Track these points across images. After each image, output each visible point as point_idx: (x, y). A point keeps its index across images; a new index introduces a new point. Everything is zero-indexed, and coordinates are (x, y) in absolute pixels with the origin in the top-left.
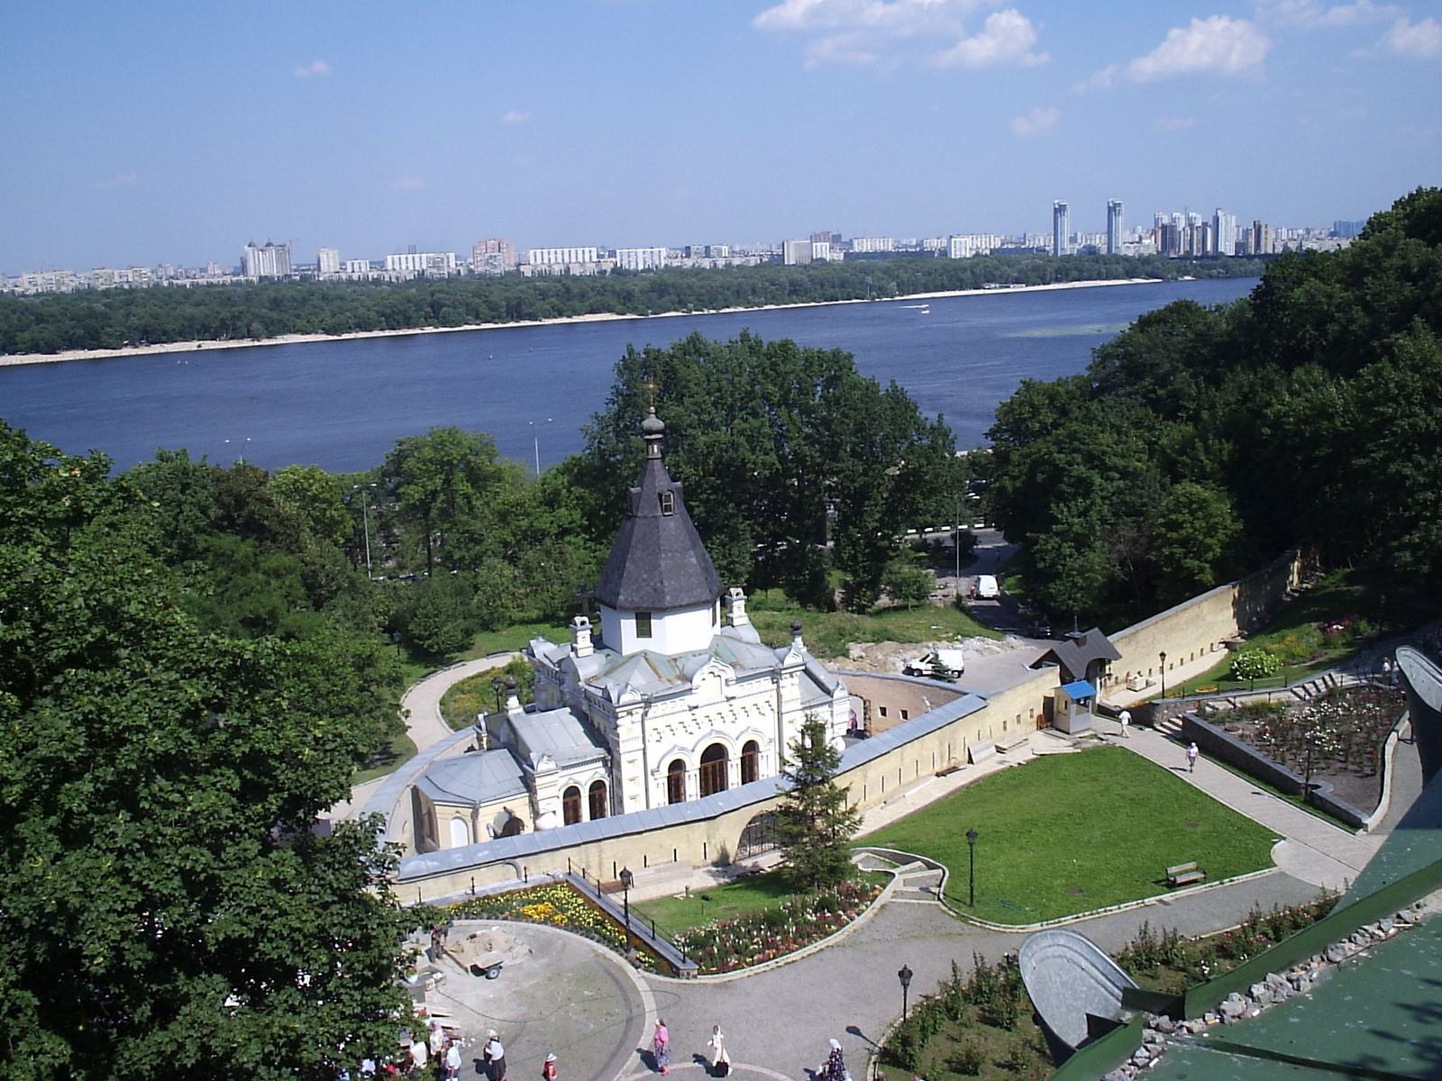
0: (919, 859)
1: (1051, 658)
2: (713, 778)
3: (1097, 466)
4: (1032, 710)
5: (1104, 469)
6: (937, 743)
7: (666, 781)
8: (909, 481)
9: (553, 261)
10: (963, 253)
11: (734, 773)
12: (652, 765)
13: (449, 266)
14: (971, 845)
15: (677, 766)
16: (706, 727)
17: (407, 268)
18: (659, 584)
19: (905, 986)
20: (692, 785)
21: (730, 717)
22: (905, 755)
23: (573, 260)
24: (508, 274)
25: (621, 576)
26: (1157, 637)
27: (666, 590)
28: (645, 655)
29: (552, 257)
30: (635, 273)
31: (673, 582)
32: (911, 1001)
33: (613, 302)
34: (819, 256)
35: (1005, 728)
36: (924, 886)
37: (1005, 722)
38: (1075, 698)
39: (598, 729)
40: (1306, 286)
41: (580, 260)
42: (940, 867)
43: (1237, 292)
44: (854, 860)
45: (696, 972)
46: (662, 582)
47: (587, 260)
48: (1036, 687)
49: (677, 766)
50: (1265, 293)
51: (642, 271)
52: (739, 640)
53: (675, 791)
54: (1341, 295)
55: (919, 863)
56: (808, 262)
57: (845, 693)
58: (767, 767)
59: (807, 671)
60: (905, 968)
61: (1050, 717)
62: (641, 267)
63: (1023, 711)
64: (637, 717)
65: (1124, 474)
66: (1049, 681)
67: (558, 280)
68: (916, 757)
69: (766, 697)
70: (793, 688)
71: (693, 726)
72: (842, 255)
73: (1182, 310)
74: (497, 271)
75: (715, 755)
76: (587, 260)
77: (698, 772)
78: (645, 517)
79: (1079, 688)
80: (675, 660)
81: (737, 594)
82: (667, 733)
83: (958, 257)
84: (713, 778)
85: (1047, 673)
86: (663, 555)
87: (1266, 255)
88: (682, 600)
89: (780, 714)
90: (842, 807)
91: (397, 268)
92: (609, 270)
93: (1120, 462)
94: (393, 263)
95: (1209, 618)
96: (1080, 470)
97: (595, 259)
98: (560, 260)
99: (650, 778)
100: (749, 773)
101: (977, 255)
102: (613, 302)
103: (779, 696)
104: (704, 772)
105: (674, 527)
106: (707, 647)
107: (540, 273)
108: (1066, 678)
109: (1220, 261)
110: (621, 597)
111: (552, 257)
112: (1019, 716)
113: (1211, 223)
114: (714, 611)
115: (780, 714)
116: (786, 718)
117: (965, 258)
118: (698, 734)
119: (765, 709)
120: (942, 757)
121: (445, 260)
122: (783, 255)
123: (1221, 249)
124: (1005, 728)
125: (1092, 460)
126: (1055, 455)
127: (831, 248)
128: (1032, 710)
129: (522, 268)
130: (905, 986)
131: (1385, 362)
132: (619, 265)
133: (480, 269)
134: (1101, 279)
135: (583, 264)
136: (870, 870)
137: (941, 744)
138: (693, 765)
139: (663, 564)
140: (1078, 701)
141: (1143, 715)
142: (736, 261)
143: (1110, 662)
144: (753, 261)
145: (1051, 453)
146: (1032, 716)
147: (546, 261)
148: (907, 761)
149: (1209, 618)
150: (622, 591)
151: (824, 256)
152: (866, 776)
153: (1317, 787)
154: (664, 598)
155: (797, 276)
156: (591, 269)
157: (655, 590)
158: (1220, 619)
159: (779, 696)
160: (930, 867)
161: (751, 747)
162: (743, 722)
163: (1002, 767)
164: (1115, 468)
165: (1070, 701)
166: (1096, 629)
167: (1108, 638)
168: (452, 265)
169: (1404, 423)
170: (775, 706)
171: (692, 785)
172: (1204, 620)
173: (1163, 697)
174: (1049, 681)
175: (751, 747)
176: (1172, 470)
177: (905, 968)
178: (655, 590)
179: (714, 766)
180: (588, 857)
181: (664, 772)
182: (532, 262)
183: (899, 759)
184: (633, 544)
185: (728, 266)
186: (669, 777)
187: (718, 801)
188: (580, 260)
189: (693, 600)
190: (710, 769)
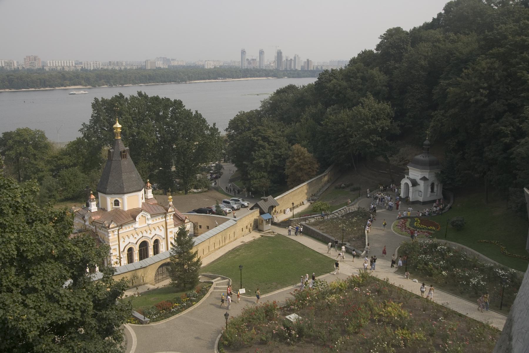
0: (220, 277)
1: (256, 206)
2: (143, 254)
3: (267, 141)
5: (269, 142)
6: (221, 236)
7: (126, 255)
8: (201, 149)
9: (57, 65)
11: (151, 252)
12: (122, 250)
13: (14, 66)
14: (241, 270)
15: (130, 250)
16: (140, 235)
17: (72, 65)
18: (122, 185)
20: (136, 257)
21: (149, 232)
23: (65, 65)
24: (39, 69)
25: (107, 182)
27: (124, 186)
29: (57, 63)
30: (90, 71)
32: (229, 321)
33: (83, 82)
34: (159, 66)
35: (242, 231)
38: (265, 219)
41: (68, 65)
42: (227, 279)
45: (149, 322)
46: (123, 184)
47: (71, 65)
48: (252, 216)
49: (130, 250)
50: (319, 83)
53: (130, 259)
54: (345, 84)
55: (219, 278)
56: (155, 68)
58: (162, 248)
61: (257, 226)
62: (92, 68)
64: (116, 233)
66: (256, 214)
67: (60, 72)
68: (214, 242)
69: (162, 223)
72: (167, 66)
73: (291, 88)
74: (35, 68)
75: (144, 245)
76: (71, 65)
77: (138, 251)
78: (116, 160)
82: (127, 238)
83: (208, 68)
84: (143, 254)
85: (256, 211)
86: (123, 174)
87: (311, 71)
88: (130, 190)
90: (195, 259)
91: (63, 65)
92: (80, 69)
93: (274, 140)
94: (64, 63)
96: (261, 142)
97: (74, 65)
98: (60, 65)
100: (156, 251)
101: (215, 68)
103: (166, 223)
104: (140, 251)
107: (52, 69)
108: (262, 213)
109: (296, 72)
110: (108, 190)
111: (57, 63)
113: (293, 59)
115: (167, 229)
116: (169, 230)
117: (211, 68)
118: (138, 238)
119: (161, 228)
121: (12, 63)
122: (146, 65)
123: (297, 68)
124: (242, 231)
125: (265, 139)
126: (253, 137)
127: (163, 64)
128: (251, 224)
129: (45, 68)
131: (360, 106)
132: (83, 67)
133: (27, 67)
134: (255, 77)
135: (69, 67)
136: (203, 281)
137: (222, 237)
140: (266, 220)
142: (128, 68)
143: (275, 206)
144: (134, 68)
145: (251, 137)
146: (251, 226)
147: (54, 65)
148: (211, 243)
150: (108, 187)
151: (161, 66)
154: (124, 189)
156: (72, 69)
157: (120, 187)
159: (166, 223)
160: (224, 279)
161: (156, 242)
162: (153, 233)
163: (243, 243)
164: (272, 142)
165: (263, 221)
166: (271, 196)
167: (275, 198)
168: (16, 65)
169: (366, 127)
170: (165, 227)
171: (136, 257)
173: (293, 218)
174: (256, 214)
175: (156, 242)
178: (120, 187)
179: (144, 249)
180: (207, 253)
182: (49, 65)
183: (208, 243)
184: (111, 170)
186: (128, 254)
187: (146, 262)
188: (68, 65)
189: (134, 190)
190: (145, 249)
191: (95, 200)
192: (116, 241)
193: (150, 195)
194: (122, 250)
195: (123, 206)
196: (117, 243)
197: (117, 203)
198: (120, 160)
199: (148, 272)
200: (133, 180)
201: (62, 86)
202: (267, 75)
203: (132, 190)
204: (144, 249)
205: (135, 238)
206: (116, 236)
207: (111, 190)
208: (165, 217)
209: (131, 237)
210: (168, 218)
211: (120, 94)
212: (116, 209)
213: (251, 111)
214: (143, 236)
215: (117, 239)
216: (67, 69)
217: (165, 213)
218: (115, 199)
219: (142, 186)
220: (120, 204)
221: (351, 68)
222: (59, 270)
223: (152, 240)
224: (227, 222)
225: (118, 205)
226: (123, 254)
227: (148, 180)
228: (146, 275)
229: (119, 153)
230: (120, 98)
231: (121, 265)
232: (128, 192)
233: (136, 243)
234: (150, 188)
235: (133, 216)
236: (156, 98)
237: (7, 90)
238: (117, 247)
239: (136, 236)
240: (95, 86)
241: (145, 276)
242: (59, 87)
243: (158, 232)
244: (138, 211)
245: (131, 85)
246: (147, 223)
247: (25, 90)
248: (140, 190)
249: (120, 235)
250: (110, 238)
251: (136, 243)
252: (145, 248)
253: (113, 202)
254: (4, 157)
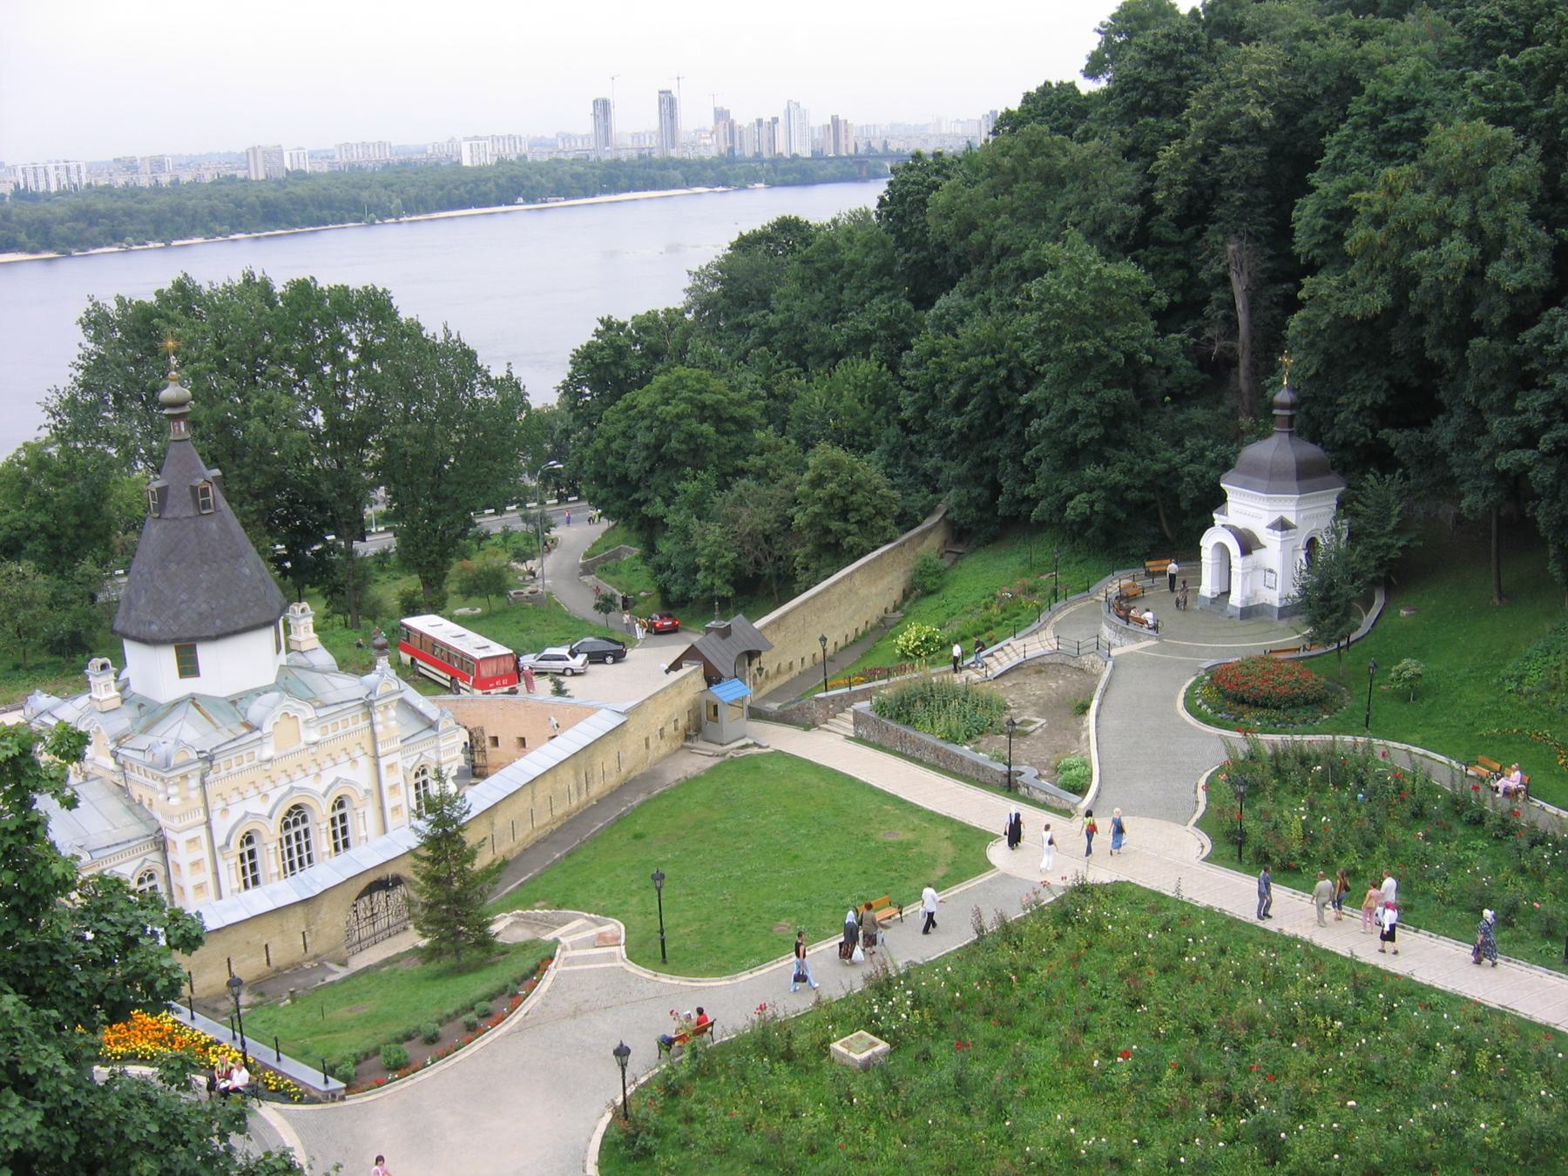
4: (676, 721)
6: (572, 772)
10: (483, 160)
11: (322, 841)
12: (220, 840)
19: (623, 1066)
20: (270, 861)
22: (536, 792)
26: (808, 619)
28: (193, 700)
30: (47, 196)
35: (647, 746)
36: (935, 918)
37: (647, 739)
39: (140, 803)
43: (866, 197)
44: (494, 928)
51: (59, 193)
52: (312, 669)
53: (251, 877)
57: (452, 723)
59: (403, 703)
60: (622, 1045)
62: (54, 188)
63: (666, 724)
64: (194, 782)
70: (390, 722)
71: (267, 787)
75: (296, 815)
80: (234, 703)
81: (303, 611)
89: (376, 757)
95: (863, 592)
99: (219, 857)
102: (23, 237)
106: (272, 681)
112: (662, 730)
113: (782, 118)
114: (277, 632)
115: (376, 757)
116: (384, 762)
118: (275, 796)
120: (579, 790)
124: (647, 746)
128: (676, 721)
130: (623, 1066)
132: (22, 187)
138: (270, 835)
144: (208, 178)
146: (676, 729)
148: (539, 799)
149: (863, 592)
151: (302, 167)
152: (492, 824)
153: (1021, 774)
155: (271, 195)
158: (874, 590)
171: (270, 861)
172: (856, 593)
181: (235, 848)
183: (529, 798)
185: (175, 183)
189: (250, 622)
194: (220, 840)
199: (322, 913)
200: (244, 585)
203: (242, 625)
206: (196, 795)
214: (292, 789)
233: (325, 795)
241: (309, 931)
243: (345, 771)
251: (270, 817)
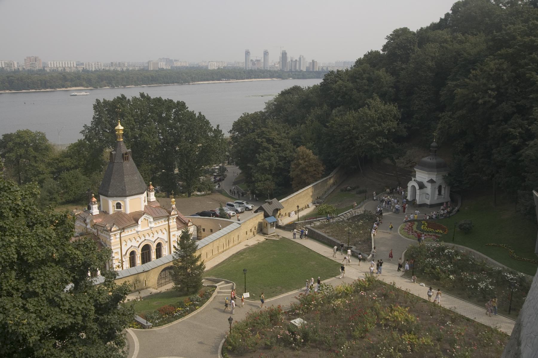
0: (223, 280)
1: (261, 209)
2: (146, 258)
3: (271, 143)
5: (274, 144)
6: (225, 240)
7: (129, 259)
8: (205, 151)
9: (58, 66)
11: (153, 256)
12: (124, 253)
13: (14, 67)
14: (245, 274)
15: (133, 254)
16: (143, 239)
18: (124, 187)
20: (138, 261)
21: (152, 235)
23: (67, 66)
24: (40, 70)
25: (109, 185)
27: (127, 189)
29: (58, 64)
30: (92, 72)
31: (129, 186)
32: (233, 325)
33: (84, 83)
34: (162, 67)
35: (247, 234)
38: (270, 222)
40: (338, 83)
41: (69, 66)
42: (231, 283)
45: (151, 326)
46: (125, 186)
47: (72, 66)
48: (257, 219)
49: (133, 254)
50: (324, 85)
53: (133, 263)
58: (165, 252)
61: (261, 229)
62: (94, 69)
64: (118, 236)
65: (280, 145)
66: (260, 217)
67: (61, 73)
68: (218, 245)
69: (165, 227)
72: (170, 67)
73: (296, 89)
74: (36, 69)
75: (146, 249)
76: (72, 66)
77: (140, 255)
78: (118, 162)
79: (271, 220)
82: (129, 242)
83: (212, 69)
84: (146, 258)
85: (260, 214)
86: (125, 177)
87: (317, 72)
88: (133, 193)
92: (81, 70)
93: (279, 142)
94: (65, 64)
96: (265, 144)
97: (75, 66)
98: (61, 66)
100: (159, 254)
101: (219, 68)
103: (169, 226)
104: (143, 255)
105: (130, 165)
107: (53, 70)
108: (266, 216)
110: (109, 192)
111: (58, 64)
113: (298, 60)
115: (169, 232)
116: (172, 234)
117: (214, 69)
118: (140, 241)
119: (164, 231)
122: (148, 66)
123: (302, 69)
124: (247, 234)
125: (269, 141)
126: (257, 139)
128: (255, 227)
129: (46, 69)
131: (366, 107)
132: (85, 68)
133: (28, 68)
134: (259, 78)
135: (70, 68)
136: (207, 285)
137: (226, 240)
139: (125, 179)
140: (271, 223)
141: (290, 227)
142: (131, 69)
143: (280, 209)
144: (137, 69)
145: (255, 139)
147: (55, 66)
148: (215, 247)
150: (110, 190)
151: (163, 67)
154: (126, 192)
156: (74, 70)
157: (122, 189)
159: (169, 226)
160: (227, 283)
161: (159, 245)
162: (156, 236)
163: (247, 247)
164: (277, 144)
166: (275, 199)
167: (279, 201)
168: (16, 66)
170: (167, 230)
171: (138, 261)
173: (298, 221)
174: (260, 217)
175: (159, 245)
176: (297, 143)
177: (230, 317)
178: (122, 189)
179: (146, 253)
182: (50, 66)
184: (113, 173)
186: (130, 258)
187: (148, 265)
188: (69, 66)
189: (137, 192)
190: (147, 253)
191: (96, 202)
192: (118, 244)
193: (153, 198)
194: (124, 253)
195: (125, 209)
196: (119, 246)
197: (119, 206)
198: (122, 162)
200: (136, 182)
201: (63, 87)
202: (271, 76)
204: (146, 253)
205: (138, 241)
206: (118, 239)
207: (113, 193)
208: (168, 220)
209: (133, 240)
210: (171, 221)
211: (122, 95)
212: (118, 212)
213: (255, 112)
214: (145, 240)
215: (119, 242)
216: (68, 70)
217: (168, 216)
218: (117, 202)
219: (145, 189)
220: (122, 207)
221: (357, 69)
222: (60, 274)
223: (155, 244)
224: (231, 225)
225: (120, 208)
226: (125, 258)
227: (151, 183)
228: (148, 279)
229: (121, 155)
230: (122, 99)
231: (123, 269)
232: (130, 194)
233: (139, 247)
234: (152, 191)
235: (135, 219)
236: (159, 100)
237: (7, 91)
238: (119, 250)
239: (138, 239)
240: (96, 88)
241: (147, 280)
242: (60, 88)
243: (160, 235)
244: (141, 214)
245: (133, 86)
246: (149, 226)
247: (25, 91)
248: (143, 193)
249: (122, 238)
250: (112, 241)
252: (147, 251)
253: (115, 205)
254: (4, 159)
